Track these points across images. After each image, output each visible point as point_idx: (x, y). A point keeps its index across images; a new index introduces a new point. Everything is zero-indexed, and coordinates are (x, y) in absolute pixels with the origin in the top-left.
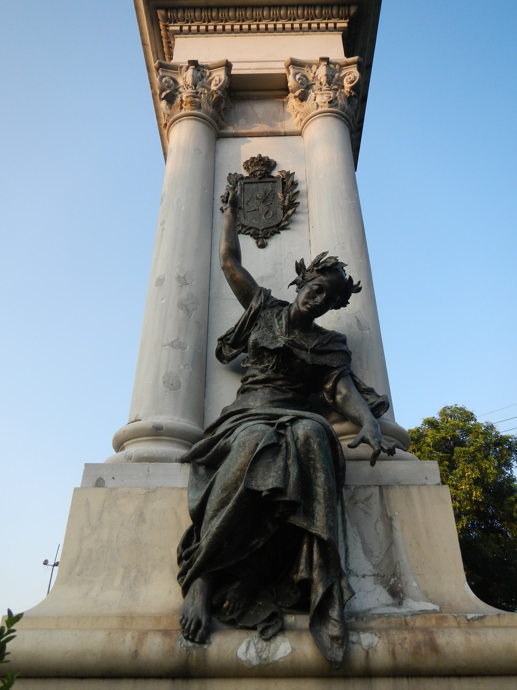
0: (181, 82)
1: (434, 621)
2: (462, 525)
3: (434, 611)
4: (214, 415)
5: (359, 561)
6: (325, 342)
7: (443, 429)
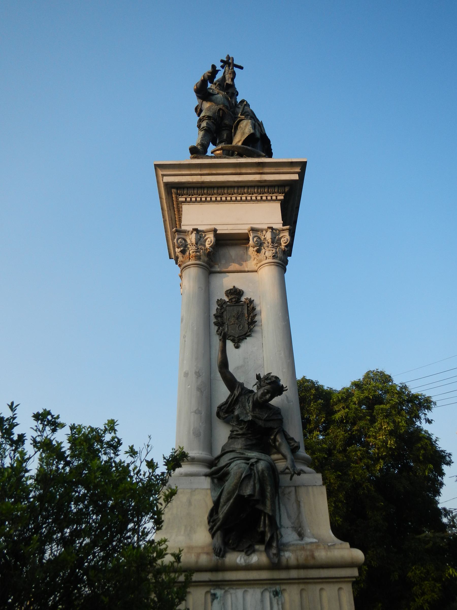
0: (189, 242)
1: (315, 547)
2: (380, 467)
3: (316, 542)
4: (218, 452)
5: (286, 522)
6: (271, 415)
7: (366, 390)
